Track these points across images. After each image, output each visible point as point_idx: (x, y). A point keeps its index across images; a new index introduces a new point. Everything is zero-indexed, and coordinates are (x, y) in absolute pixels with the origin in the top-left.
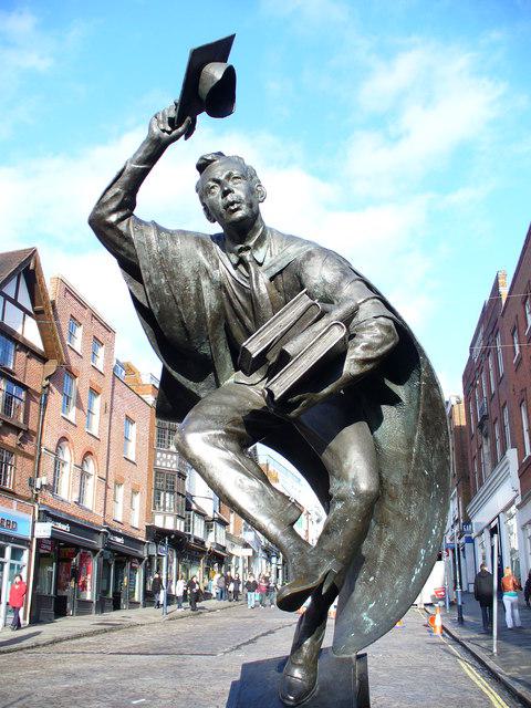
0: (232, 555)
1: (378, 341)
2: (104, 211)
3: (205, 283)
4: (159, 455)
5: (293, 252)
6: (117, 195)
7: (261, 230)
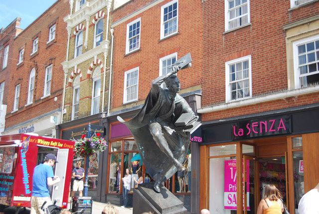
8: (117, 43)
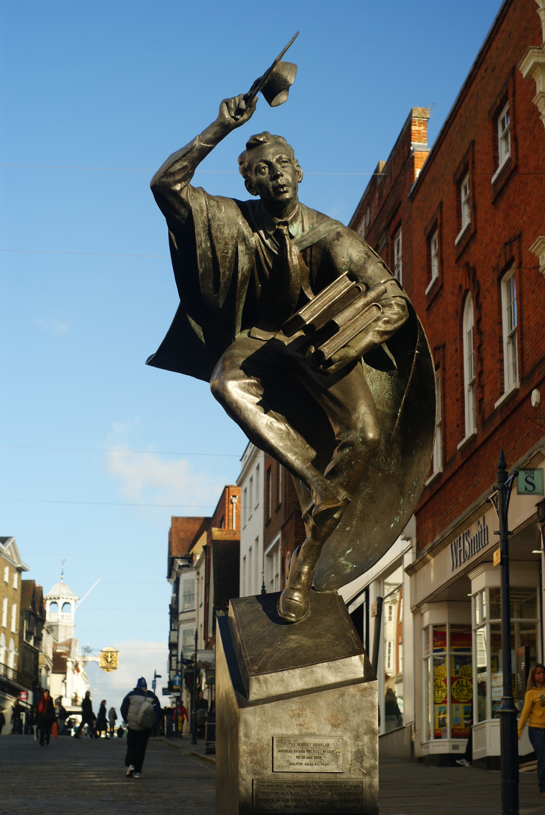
1: (395, 317)
2: (170, 180)
3: (241, 248)
5: (323, 229)
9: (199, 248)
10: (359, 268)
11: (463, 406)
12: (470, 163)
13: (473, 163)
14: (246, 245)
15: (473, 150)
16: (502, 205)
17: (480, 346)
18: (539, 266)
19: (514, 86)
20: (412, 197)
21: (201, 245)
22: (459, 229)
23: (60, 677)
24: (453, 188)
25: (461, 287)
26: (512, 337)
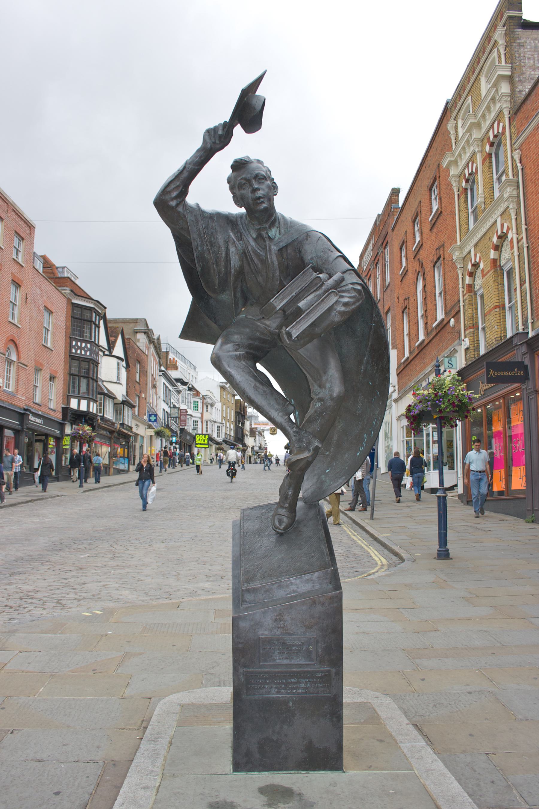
0: (137, 435)
2: (167, 197)
4: (74, 343)
6: (178, 187)
7: (274, 216)
8: (528, 178)
9: (196, 250)
10: (324, 261)
11: (418, 326)
12: (419, 212)
13: (421, 211)
14: (236, 247)
15: (420, 206)
16: (435, 231)
17: (426, 298)
18: (453, 259)
19: (439, 173)
20: (393, 229)
21: (197, 248)
22: (415, 243)
23: (253, 439)
24: (411, 224)
25: (416, 270)
26: (440, 293)
